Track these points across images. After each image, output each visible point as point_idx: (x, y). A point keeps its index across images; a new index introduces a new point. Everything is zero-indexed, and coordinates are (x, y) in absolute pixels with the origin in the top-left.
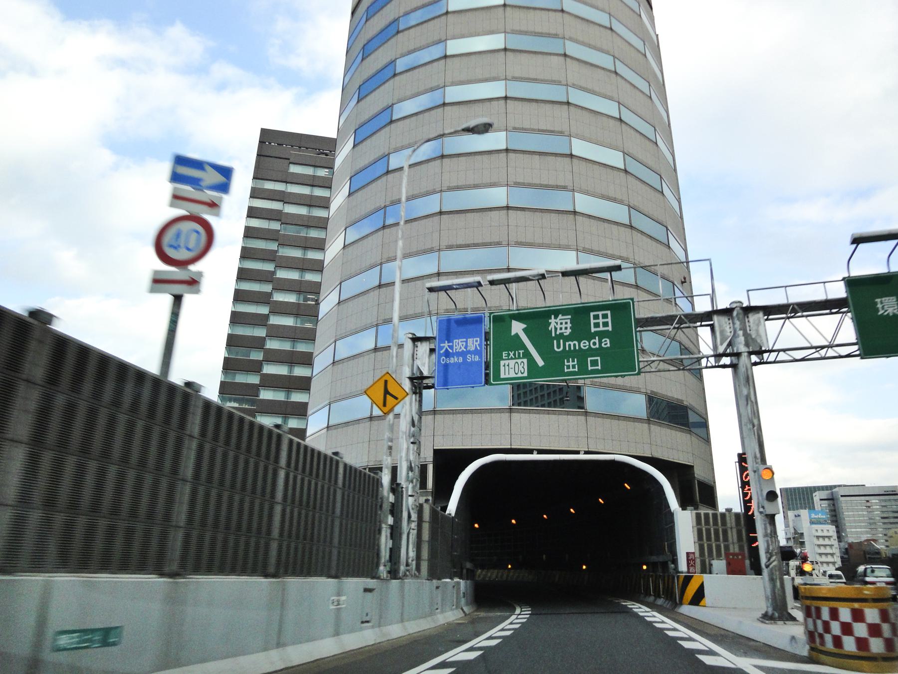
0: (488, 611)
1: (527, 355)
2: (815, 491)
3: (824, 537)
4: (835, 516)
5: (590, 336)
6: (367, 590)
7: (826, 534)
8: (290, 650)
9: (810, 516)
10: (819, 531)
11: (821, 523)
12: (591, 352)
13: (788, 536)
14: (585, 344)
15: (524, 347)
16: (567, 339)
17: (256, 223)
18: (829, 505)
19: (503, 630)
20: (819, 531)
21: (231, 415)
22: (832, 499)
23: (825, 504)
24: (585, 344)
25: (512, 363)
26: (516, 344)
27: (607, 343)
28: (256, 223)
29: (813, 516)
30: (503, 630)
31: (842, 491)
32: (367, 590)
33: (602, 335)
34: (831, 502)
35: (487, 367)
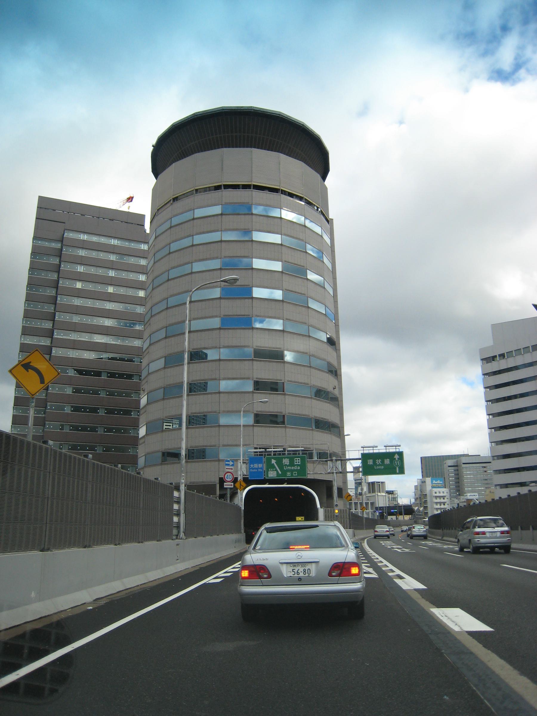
0: (131, 592)
1: (276, 470)
2: (446, 459)
3: (440, 497)
4: (458, 478)
5: (294, 466)
6: (177, 545)
7: (442, 494)
8: (125, 580)
9: (432, 482)
10: (441, 493)
11: (439, 487)
12: (294, 470)
13: (417, 497)
14: (293, 468)
15: (275, 467)
16: (288, 466)
17: (30, 340)
18: (455, 470)
19: (234, 568)
20: (441, 493)
21: (133, 476)
22: (457, 466)
23: (452, 469)
24: (293, 468)
25: (272, 472)
26: (273, 466)
27: (299, 468)
28: (30, 340)
29: (434, 482)
30: (234, 568)
31: (464, 460)
32: (177, 545)
33: (298, 465)
34: (456, 468)
35: (265, 472)
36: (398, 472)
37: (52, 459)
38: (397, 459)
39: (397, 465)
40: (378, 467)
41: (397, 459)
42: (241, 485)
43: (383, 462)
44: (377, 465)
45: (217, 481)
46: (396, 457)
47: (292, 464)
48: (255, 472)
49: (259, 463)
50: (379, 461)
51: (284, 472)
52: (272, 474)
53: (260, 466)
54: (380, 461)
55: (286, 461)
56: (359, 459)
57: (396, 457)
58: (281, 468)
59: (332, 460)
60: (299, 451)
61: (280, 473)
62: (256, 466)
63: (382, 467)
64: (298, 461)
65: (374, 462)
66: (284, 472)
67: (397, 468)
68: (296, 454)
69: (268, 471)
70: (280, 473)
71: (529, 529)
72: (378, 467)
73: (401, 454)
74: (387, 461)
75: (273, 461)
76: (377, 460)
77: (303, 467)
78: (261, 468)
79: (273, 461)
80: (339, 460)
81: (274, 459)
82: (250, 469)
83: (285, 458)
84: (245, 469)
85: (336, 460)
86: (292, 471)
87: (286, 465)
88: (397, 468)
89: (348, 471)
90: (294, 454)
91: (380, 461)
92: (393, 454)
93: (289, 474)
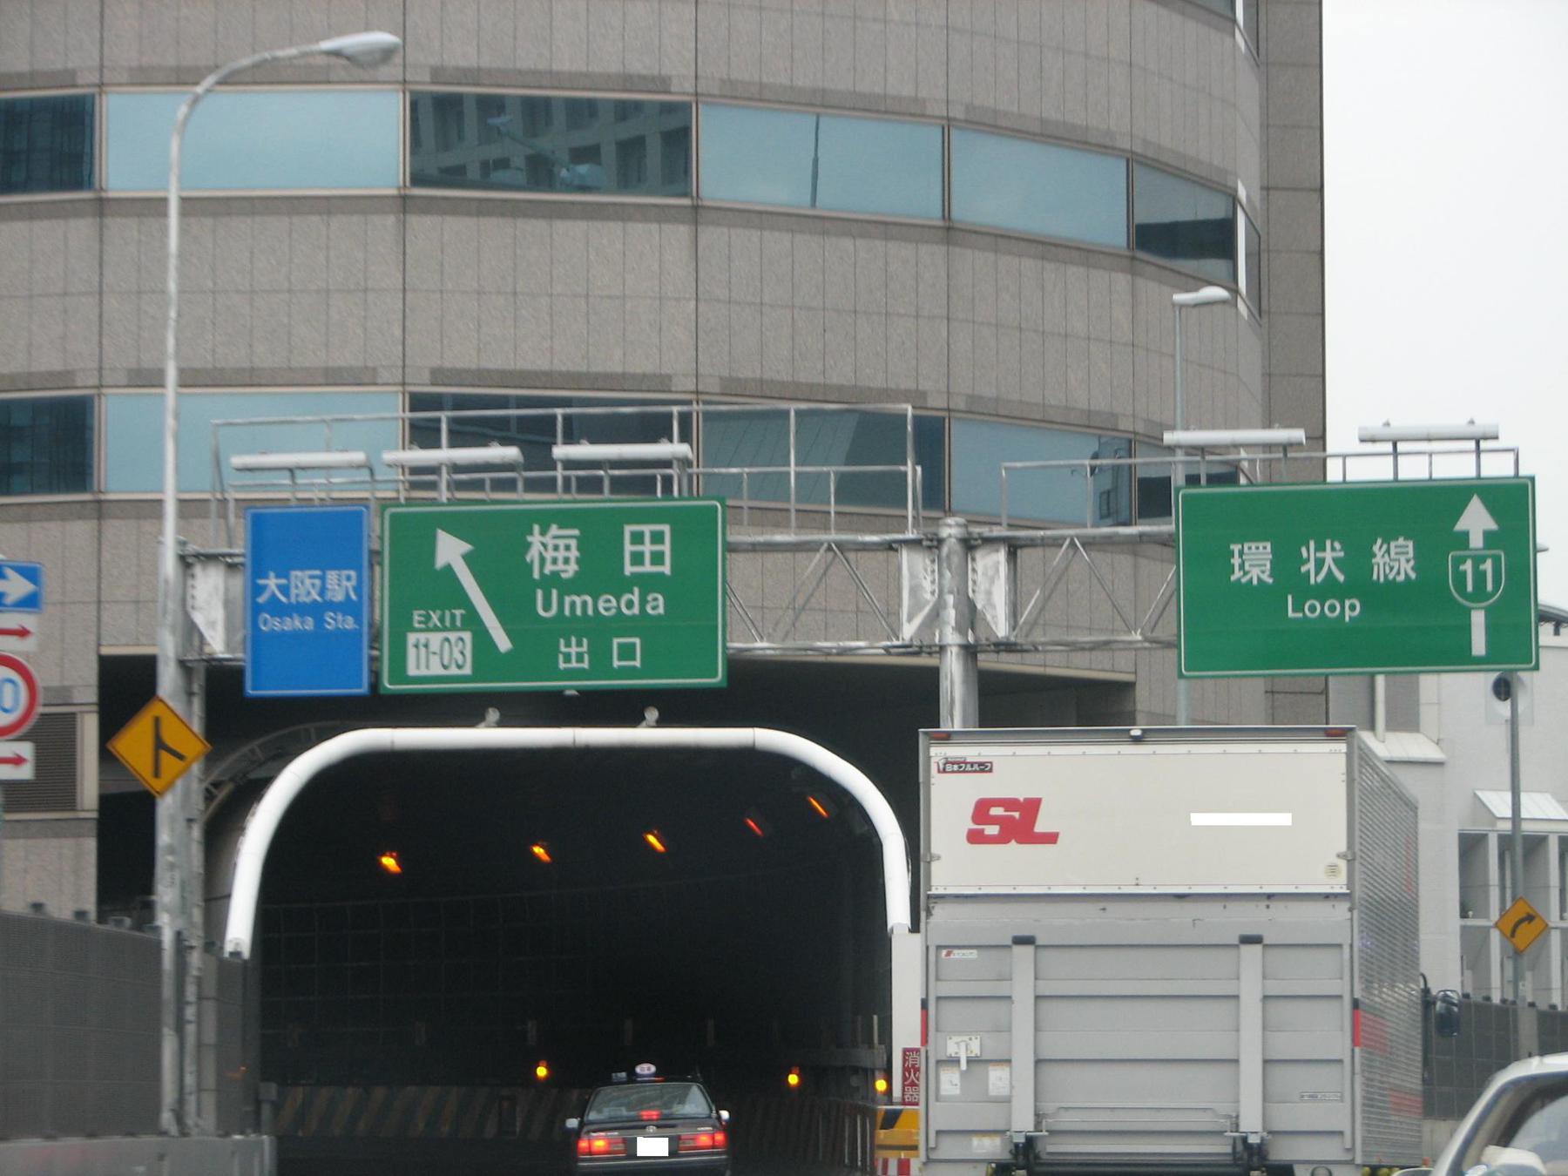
1: (472, 621)
5: (620, 585)
12: (622, 624)
14: (607, 605)
15: (464, 601)
16: (567, 587)
24: (607, 605)
25: (435, 639)
26: (446, 592)
27: (657, 605)
33: (648, 583)
35: (376, 638)
36: (1479, 646)
37: (377, 593)
38: (1476, 541)
39: (1480, 593)
40: (1313, 610)
41: (1476, 541)
42: (160, 745)
43: (1356, 560)
44: (1304, 591)
45: (86, 689)
46: (1476, 521)
47: (600, 569)
48: (296, 635)
49: (323, 562)
50: (1323, 560)
51: (536, 639)
52: (436, 657)
53: (340, 584)
54: (1331, 553)
55: (553, 551)
56: (1136, 567)
57: (1476, 521)
58: (512, 607)
59: (933, 544)
60: (667, 463)
61: (503, 643)
62: (304, 585)
63: (1352, 610)
64: (648, 548)
65: (1285, 562)
66: (536, 639)
67: (1478, 619)
68: (644, 486)
69: (402, 625)
70: (503, 643)
71: (412, 410)
72: (1313, 610)
73: (1512, 501)
74: (1395, 560)
75: (450, 550)
76: (1309, 552)
77: (694, 589)
78: (348, 607)
79: (450, 550)
80: (989, 541)
81: (458, 525)
82: (257, 609)
83: (546, 520)
84: (218, 614)
85: (969, 545)
86: (597, 630)
87: (553, 580)
88: (1478, 619)
89: (825, 123)
90: (619, 485)
91: (1331, 553)
92: (1452, 496)
93: (573, 655)
